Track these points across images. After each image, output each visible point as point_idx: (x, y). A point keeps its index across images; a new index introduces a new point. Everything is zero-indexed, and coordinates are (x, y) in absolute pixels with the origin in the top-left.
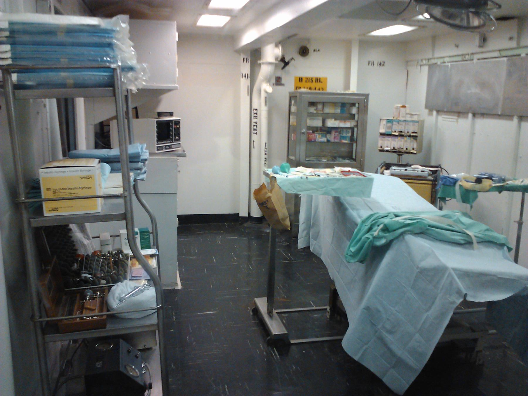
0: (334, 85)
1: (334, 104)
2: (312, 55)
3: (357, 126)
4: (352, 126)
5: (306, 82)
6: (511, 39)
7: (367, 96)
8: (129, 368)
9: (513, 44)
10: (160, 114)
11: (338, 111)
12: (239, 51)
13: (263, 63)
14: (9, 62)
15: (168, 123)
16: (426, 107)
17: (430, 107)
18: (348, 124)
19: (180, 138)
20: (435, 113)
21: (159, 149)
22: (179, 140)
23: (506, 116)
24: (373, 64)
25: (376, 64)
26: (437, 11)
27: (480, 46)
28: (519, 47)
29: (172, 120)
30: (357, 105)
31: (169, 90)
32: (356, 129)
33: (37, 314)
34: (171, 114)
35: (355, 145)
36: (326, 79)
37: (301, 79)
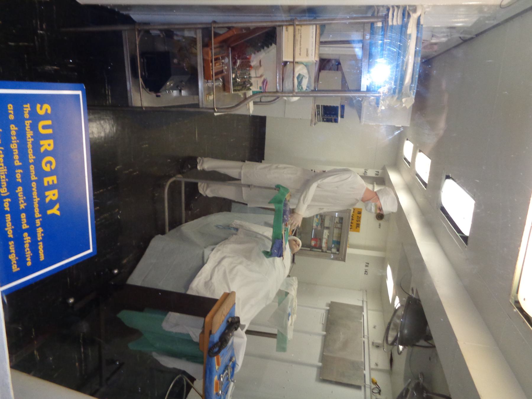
0: (353, 237)
1: (340, 236)
2: (377, 222)
3: (322, 251)
4: (323, 248)
5: (358, 217)
6: (377, 365)
7: (344, 260)
8: (171, 82)
9: (373, 366)
10: (343, 107)
11: (335, 239)
12: (384, 169)
13: (374, 186)
14: (390, 23)
15: (336, 114)
16: (332, 302)
17: (332, 306)
18: (324, 245)
19: (325, 121)
20: (328, 308)
21: (318, 107)
22: (323, 121)
23: (323, 358)
24: (366, 266)
25: (367, 268)
26: (401, 312)
27: (373, 343)
28: (371, 369)
29: (338, 117)
30: (337, 253)
31: (360, 117)
32: (320, 250)
33: (217, 26)
34: (342, 116)
35: (309, 249)
36: (359, 231)
37: (360, 213)
